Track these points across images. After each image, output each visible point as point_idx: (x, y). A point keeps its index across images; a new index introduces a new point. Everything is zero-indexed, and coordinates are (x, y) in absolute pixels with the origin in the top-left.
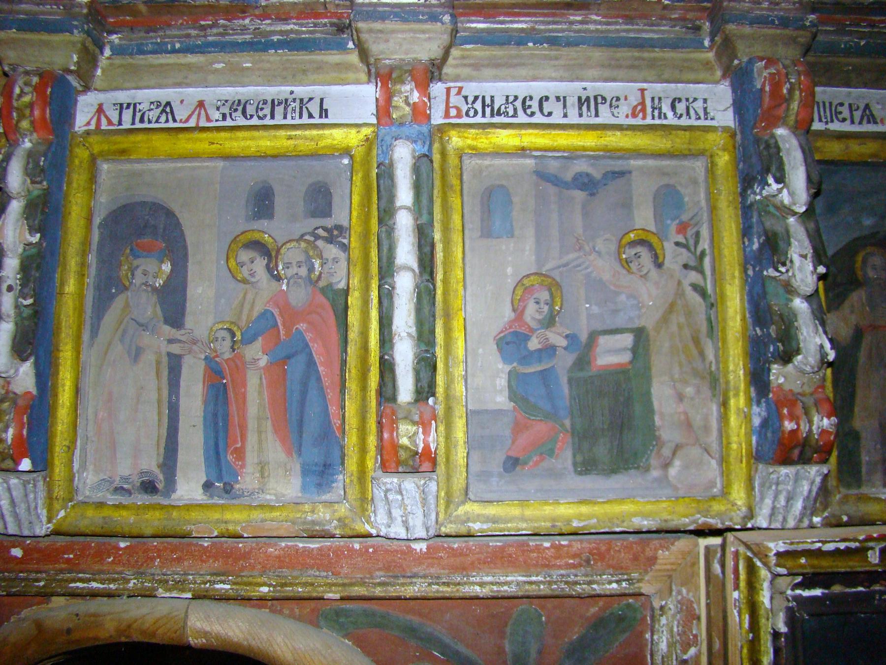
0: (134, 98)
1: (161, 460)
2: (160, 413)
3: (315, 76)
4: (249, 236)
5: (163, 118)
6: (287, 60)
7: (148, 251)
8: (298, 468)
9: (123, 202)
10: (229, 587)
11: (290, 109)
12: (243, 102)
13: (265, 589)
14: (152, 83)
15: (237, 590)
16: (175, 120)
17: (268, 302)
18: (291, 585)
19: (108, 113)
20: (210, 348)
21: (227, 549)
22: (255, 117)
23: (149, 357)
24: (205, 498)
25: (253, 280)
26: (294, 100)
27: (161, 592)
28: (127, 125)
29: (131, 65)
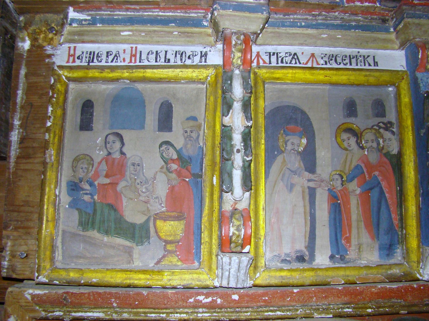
0: (276, 50)
1: (307, 244)
2: (305, 219)
3: (372, 45)
4: (345, 126)
5: (294, 62)
6: (359, 35)
7: (293, 132)
8: (377, 246)
9: (277, 105)
10: (351, 310)
11: (359, 61)
12: (334, 56)
13: (369, 310)
14: (287, 43)
15: (355, 311)
16: (300, 63)
17: (358, 160)
18: (383, 307)
19: (262, 57)
20: (330, 185)
21: (351, 290)
22: (342, 64)
23: (298, 189)
24: (331, 264)
25: (350, 149)
26: (360, 56)
27: (316, 315)
28: (274, 64)
29: (278, 33)
